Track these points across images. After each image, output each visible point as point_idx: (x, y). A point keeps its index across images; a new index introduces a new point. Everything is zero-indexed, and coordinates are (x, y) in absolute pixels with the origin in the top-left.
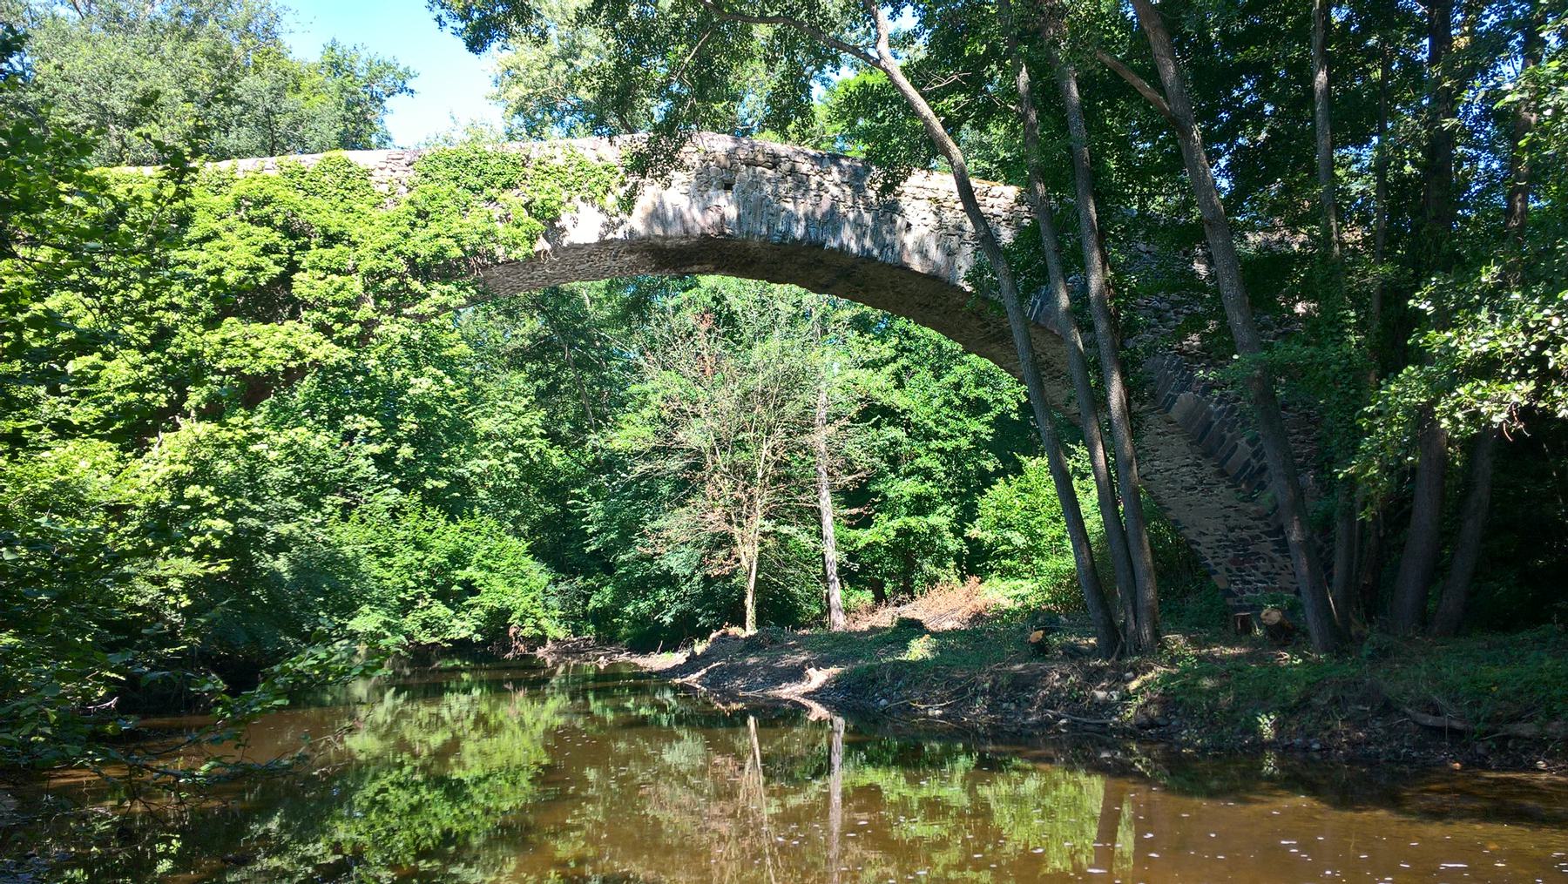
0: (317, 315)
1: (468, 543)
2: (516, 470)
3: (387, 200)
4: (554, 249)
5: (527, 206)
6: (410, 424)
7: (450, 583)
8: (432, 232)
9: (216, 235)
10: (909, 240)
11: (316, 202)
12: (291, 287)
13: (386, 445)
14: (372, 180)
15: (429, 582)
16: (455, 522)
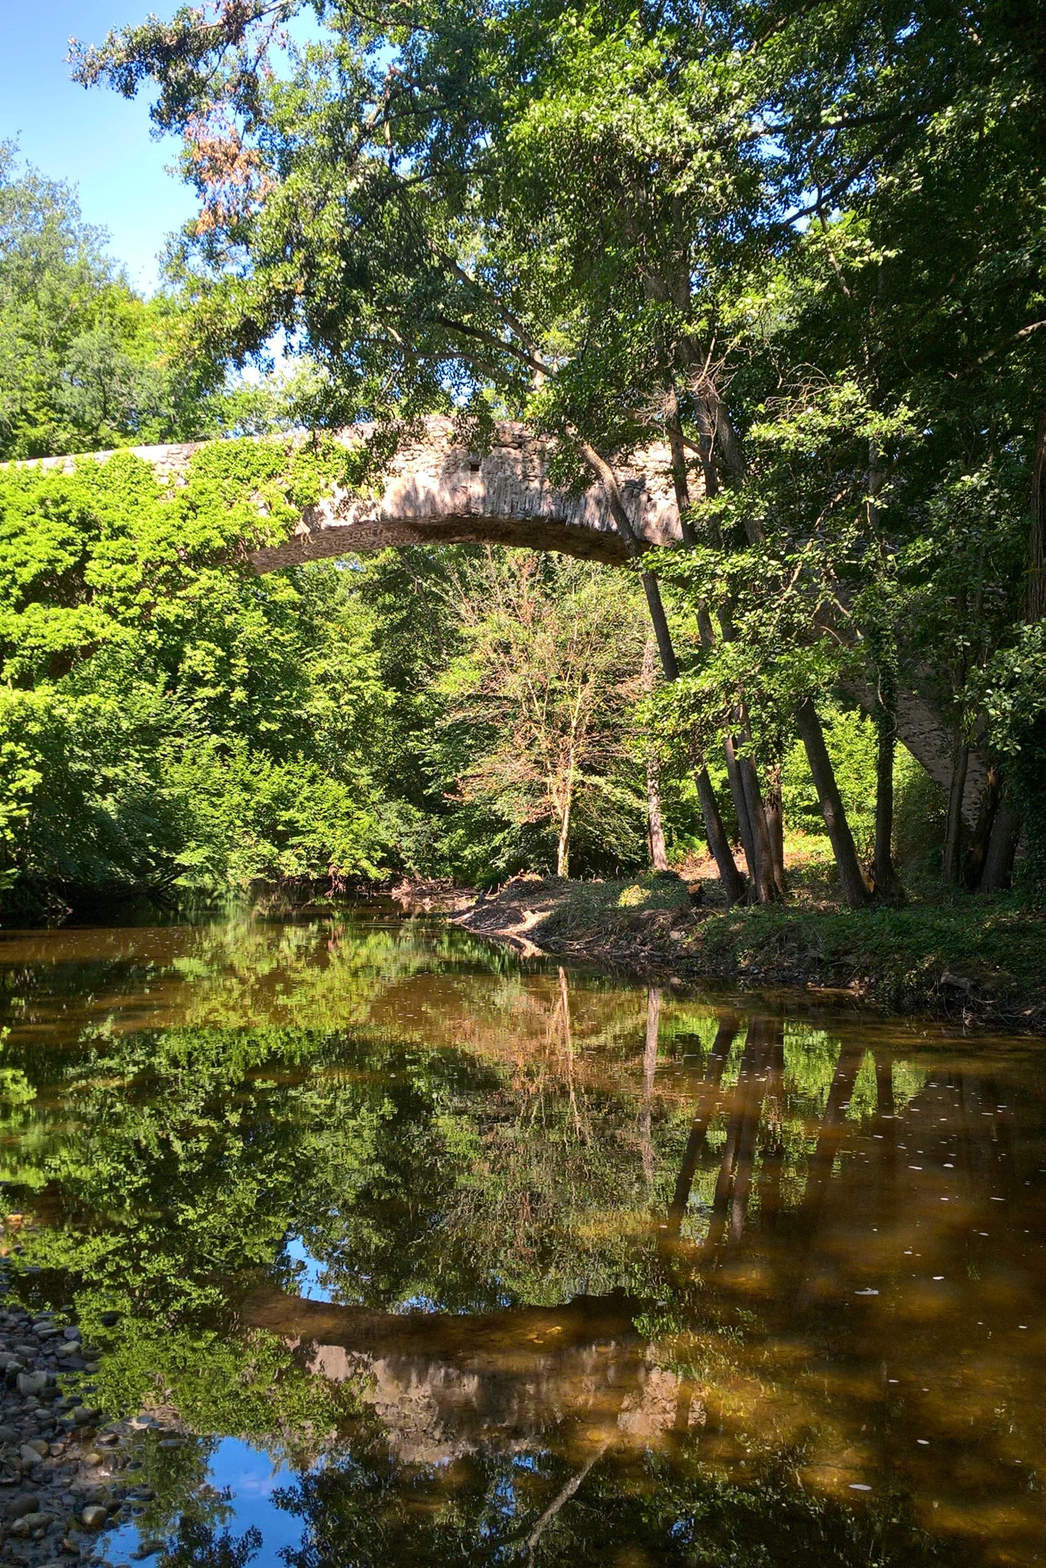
0: (105, 598)
1: (292, 786)
2: (352, 712)
3: (167, 492)
4: (312, 532)
5: (288, 494)
6: (241, 667)
7: (276, 822)
8: (200, 524)
9: (22, 531)
10: (652, 517)
11: (105, 497)
12: (83, 575)
13: (220, 689)
14: (155, 474)
15: (257, 822)
16: (280, 765)
